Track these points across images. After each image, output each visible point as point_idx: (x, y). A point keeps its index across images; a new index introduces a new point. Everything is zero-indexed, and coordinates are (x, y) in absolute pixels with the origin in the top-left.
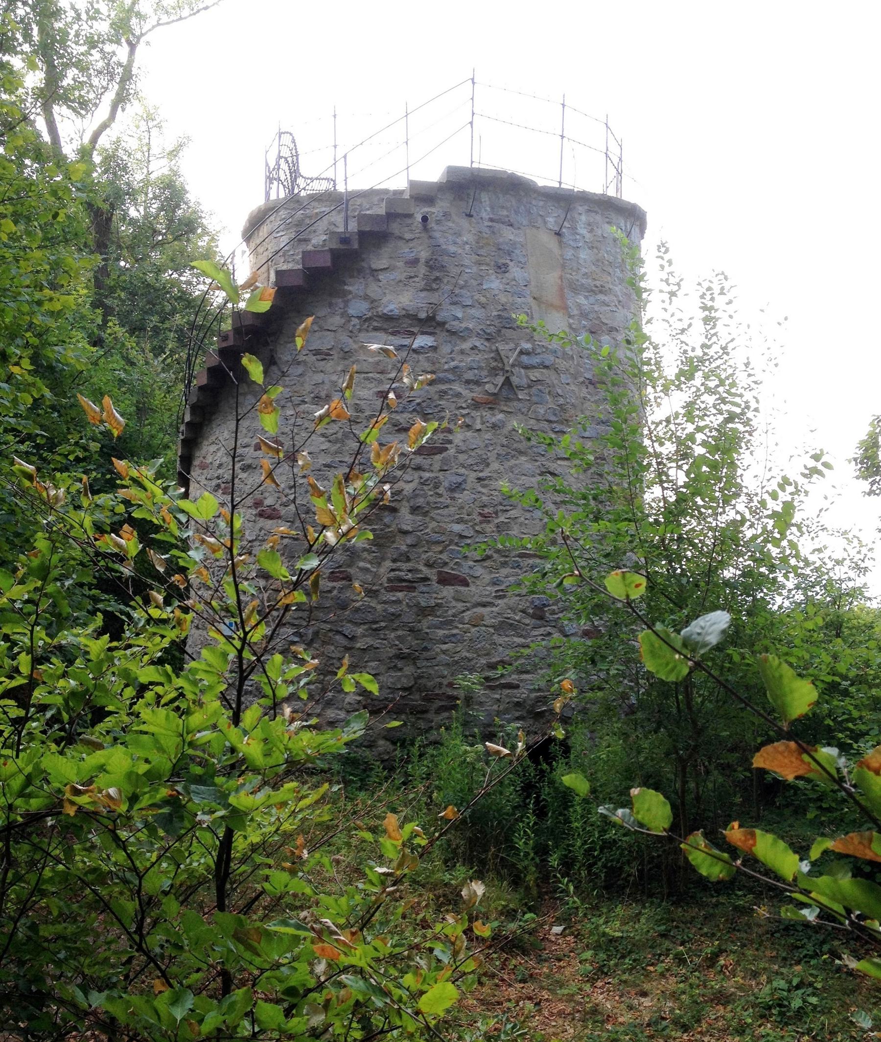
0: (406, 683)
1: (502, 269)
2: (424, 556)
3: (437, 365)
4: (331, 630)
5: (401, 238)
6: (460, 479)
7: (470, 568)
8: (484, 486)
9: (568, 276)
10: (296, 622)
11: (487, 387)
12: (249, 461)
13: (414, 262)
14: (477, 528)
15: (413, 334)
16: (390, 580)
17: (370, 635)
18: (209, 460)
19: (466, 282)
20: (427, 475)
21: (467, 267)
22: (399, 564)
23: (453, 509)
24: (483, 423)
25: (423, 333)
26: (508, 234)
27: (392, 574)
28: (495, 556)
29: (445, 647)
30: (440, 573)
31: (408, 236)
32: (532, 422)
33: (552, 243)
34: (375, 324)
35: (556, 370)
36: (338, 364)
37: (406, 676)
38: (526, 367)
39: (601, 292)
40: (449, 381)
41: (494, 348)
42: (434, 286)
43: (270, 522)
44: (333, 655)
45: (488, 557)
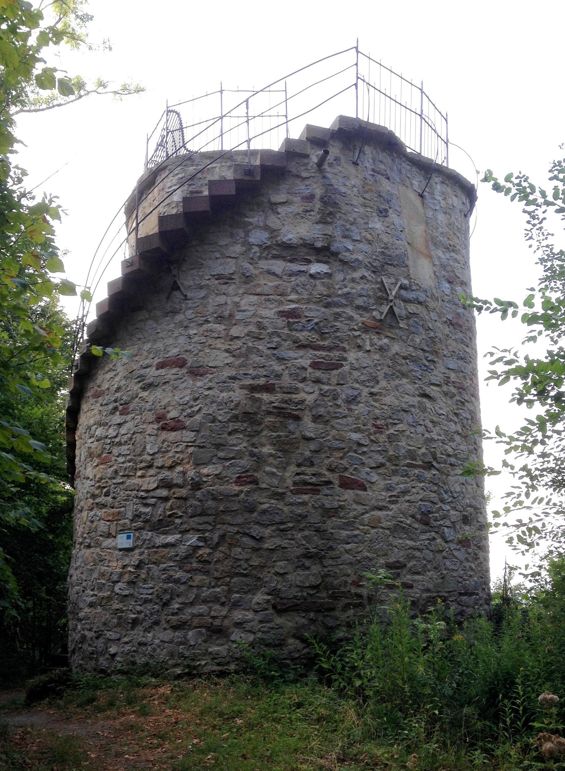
0: (313, 581)
1: (383, 213)
2: (327, 462)
3: (332, 290)
4: (238, 533)
5: (298, 176)
6: (356, 393)
7: (368, 474)
8: (376, 401)
10: (201, 527)
11: (374, 313)
12: (151, 380)
13: (310, 198)
14: (372, 437)
15: (309, 262)
16: (295, 483)
17: (278, 536)
18: (105, 386)
19: (355, 219)
20: (326, 388)
21: (355, 206)
22: (303, 468)
23: (350, 419)
24: (372, 345)
25: (319, 261)
26: (386, 186)
27: (297, 478)
28: (388, 464)
29: (348, 547)
31: (304, 174)
32: (411, 349)
33: (417, 201)
34: (275, 252)
36: (239, 288)
38: (406, 301)
39: (453, 251)
41: (379, 280)
42: (329, 220)
43: (174, 434)
44: (241, 557)
45: (382, 465)
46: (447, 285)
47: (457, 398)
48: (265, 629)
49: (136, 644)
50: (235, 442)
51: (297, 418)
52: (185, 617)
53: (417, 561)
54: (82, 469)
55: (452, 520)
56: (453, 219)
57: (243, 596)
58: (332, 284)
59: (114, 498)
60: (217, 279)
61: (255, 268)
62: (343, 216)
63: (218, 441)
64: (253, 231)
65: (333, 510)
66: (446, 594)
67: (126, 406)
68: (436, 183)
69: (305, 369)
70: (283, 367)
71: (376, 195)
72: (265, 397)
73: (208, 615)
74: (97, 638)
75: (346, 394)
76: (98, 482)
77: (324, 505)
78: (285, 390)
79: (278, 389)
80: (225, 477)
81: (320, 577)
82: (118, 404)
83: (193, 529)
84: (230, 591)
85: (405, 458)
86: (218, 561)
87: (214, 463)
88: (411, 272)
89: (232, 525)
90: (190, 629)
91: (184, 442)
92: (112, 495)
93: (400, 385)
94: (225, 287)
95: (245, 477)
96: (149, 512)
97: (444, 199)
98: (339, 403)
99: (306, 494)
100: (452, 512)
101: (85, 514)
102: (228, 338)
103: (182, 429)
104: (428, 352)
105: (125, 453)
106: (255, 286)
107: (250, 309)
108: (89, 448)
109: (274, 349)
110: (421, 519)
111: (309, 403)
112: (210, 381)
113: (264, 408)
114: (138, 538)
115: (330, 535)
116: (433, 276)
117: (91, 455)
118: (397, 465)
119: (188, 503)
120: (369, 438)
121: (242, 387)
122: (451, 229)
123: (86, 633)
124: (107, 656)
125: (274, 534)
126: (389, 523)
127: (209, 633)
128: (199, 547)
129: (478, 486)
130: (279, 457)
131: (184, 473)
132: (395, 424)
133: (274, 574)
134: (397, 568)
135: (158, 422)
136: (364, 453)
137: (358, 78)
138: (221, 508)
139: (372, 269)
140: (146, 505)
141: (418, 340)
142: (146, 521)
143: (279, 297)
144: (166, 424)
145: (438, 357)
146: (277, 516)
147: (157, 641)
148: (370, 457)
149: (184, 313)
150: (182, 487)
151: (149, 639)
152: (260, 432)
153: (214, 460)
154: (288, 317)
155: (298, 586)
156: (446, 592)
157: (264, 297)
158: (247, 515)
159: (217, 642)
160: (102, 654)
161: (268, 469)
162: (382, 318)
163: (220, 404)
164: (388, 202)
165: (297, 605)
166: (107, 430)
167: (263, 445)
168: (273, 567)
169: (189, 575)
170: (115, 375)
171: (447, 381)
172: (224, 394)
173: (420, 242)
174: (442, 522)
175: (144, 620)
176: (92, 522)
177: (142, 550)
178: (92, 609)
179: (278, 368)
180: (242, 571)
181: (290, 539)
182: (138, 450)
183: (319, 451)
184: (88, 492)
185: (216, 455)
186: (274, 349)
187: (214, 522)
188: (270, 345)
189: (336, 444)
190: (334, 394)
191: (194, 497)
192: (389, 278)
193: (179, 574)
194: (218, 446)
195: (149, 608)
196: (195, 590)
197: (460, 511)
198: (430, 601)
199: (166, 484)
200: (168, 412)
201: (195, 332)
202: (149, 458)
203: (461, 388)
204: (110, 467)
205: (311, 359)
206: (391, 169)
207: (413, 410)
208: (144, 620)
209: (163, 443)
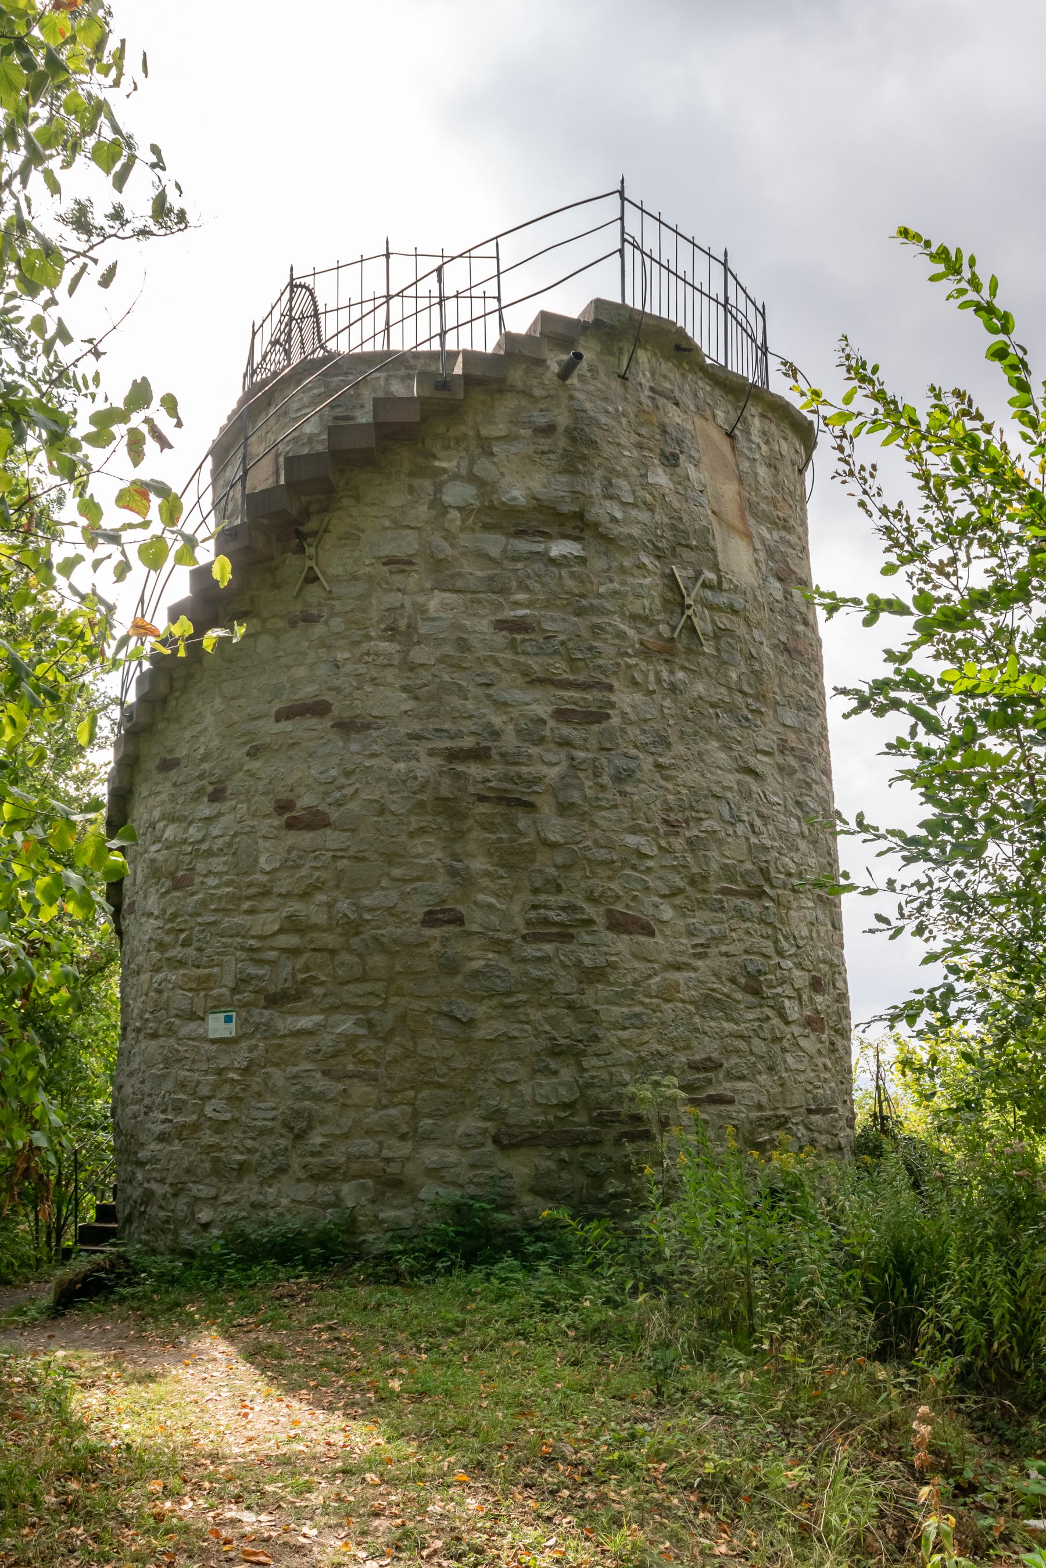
0: (566, 1095)
1: (671, 461)
4: (429, 1011)
8: (667, 778)
10: (360, 1002)
12: (268, 740)
13: (549, 430)
14: (663, 843)
21: (624, 447)
22: (543, 897)
23: (625, 811)
24: (659, 681)
27: (533, 915)
29: (625, 1035)
32: (723, 690)
33: (725, 445)
35: (747, 620)
38: (712, 608)
39: (785, 528)
40: (606, 612)
44: (434, 1055)
45: (680, 891)
46: (778, 585)
47: (799, 775)
48: (482, 1180)
49: (248, 1207)
50: (421, 850)
52: (338, 1157)
53: (740, 1057)
54: (139, 898)
55: (797, 986)
56: (781, 476)
58: (588, 576)
59: (200, 950)
60: (385, 564)
61: (452, 546)
62: (606, 463)
64: (450, 485)
66: (786, 1113)
68: (753, 416)
69: (543, 722)
70: (505, 718)
72: (474, 770)
73: (377, 1156)
74: (175, 1195)
75: (617, 767)
77: (581, 962)
81: (576, 1089)
82: (205, 782)
83: (346, 1005)
85: (719, 878)
86: (395, 1061)
87: (383, 888)
90: (347, 1178)
91: (328, 850)
92: (196, 944)
94: (398, 578)
96: (264, 975)
97: (767, 443)
98: (604, 782)
99: (550, 941)
100: (797, 973)
101: (145, 977)
103: (325, 826)
104: (751, 696)
105: (219, 869)
106: (452, 576)
107: (443, 615)
108: (153, 861)
109: (487, 685)
112: (375, 742)
113: (471, 789)
115: (594, 1015)
116: (755, 568)
118: (705, 891)
119: (338, 960)
121: (432, 753)
122: (778, 492)
123: (154, 1186)
125: (494, 1013)
128: (357, 1038)
129: (834, 926)
130: (501, 877)
131: (330, 906)
132: (701, 819)
134: (706, 1069)
136: (649, 869)
137: (623, 240)
141: (734, 676)
143: (495, 597)
144: (295, 817)
145: (766, 705)
147: (285, 1201)
149: (326, 623)
150: (325, 931)
153: (384, 883)
154: (511, 631)
155: (539, 1105)
156: (787, 1109)
157: (470, 596)
159: (395, 1203)
160: (184, 1223)
161: (481, 897)
166: (186, 829)
171: (783, 748)
172: (402, 766)
173: (731, 510)
174: (779, 990)
175: (260, 1164)
176: (159, 992)
177: (254, 1042)
178: (164, 1144)
180: (436, 1079)
181: (521, 1022)
183: (571, 866)
184: (151, 939)
186: (487, 685)
189: (602, 854)
192: (685, 568)
193: (320, 1084)
195: (269, 1142)
196: (353, 1114)
198: (762, 1126)
199: (293, 925)
200: (299, 797)
201: (347, 655)
203: (805, 760)
204: (193, 894)
205: (552, 704)
206: (681, 390)
208: (260, 1164)
209: (289, 851)
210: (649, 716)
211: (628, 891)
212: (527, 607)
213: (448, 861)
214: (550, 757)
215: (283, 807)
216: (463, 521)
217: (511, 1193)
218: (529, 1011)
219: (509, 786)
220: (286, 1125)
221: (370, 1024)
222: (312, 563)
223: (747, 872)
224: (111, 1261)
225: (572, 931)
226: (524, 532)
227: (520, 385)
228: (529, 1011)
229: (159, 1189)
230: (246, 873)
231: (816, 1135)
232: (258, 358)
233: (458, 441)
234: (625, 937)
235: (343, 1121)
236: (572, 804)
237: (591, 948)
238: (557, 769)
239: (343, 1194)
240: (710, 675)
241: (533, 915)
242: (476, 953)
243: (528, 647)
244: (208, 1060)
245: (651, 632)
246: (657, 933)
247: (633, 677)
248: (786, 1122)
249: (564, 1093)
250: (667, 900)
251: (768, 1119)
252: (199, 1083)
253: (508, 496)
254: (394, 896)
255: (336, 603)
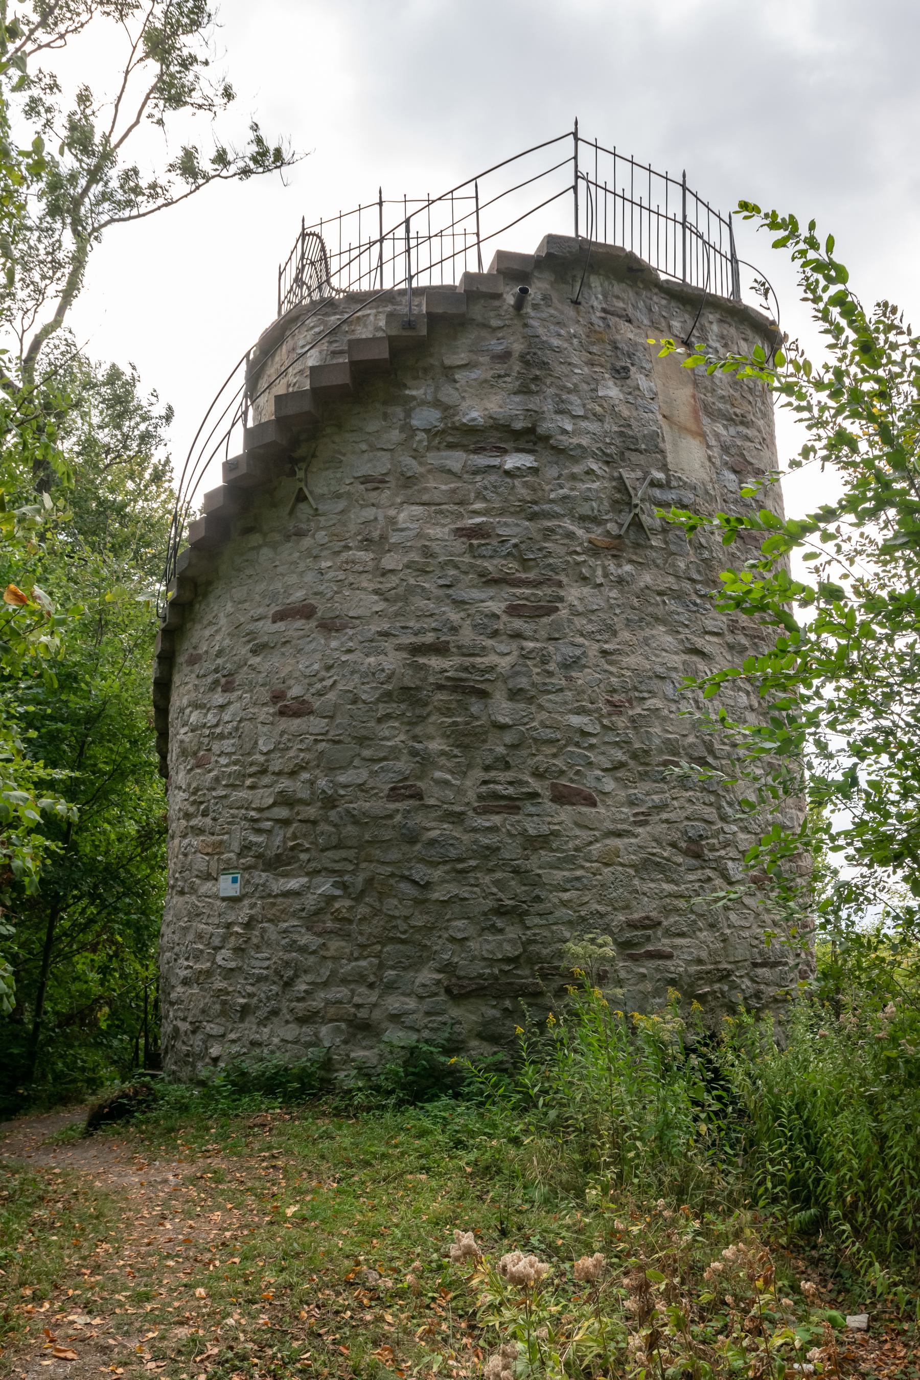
0: (510, 951)
1: (621, 374)
2: (530, 762)
3: (540, 493)
4: (392, 875)
5: (485, 326)
6: (578, 652)
7: (598, 779)
8: (610, 663)
9: (703, 396)
10: (337, 867)
11: (609, 526)
12: (265, 639)
13: (505, 356)
15: (504, 451)
16: (480, 797)
18: (204, 648)
20: (530, 645)
21: (576, 366)
22: (493, 774)
23: (569, 693)
24: (606, 575)
25: (519, 450)
26: (627, 332)
27: (484, 789)
28: (632, 763)
29: (566, 896)
30: (554, 786)
31: (495, 323)
32: (671, 579)
34: (450, 439)
36: (397, 495)
37: (510, 941)
40: (557, 516)
42: (533, 387)
43: (297, 721)
45: (621, 765)
46: (733, 477)
47: (751, 653)
48: (435, 1025)
51: (483, 694)
52: (316, 1003)
53: (680, 915)
55: (741, 849)
57: (402, 974)
58: (539, 484)
59: (214, 819)
60: (362, 483)
61: (421, 464)
62: (556, 381)
63: (364, 732)
64: (418, 410)
65: (540, 839)
66: (729, 967)
67: (230, 679)
68: (711, 323)
69: (497, 617)
70: (462, 614)
71: (609, 347)
72: (435, 662)
73: (350, 1002)
74: (194, 1032)
75: (563, 654)
76: (194, 793)
78: (464, 650)
79: (454, 650)
80: (373, 788)
81: (519, 945)
83: (326, 869)
84: (381, 966)
85: (661, 752)
86: (363, 919)
88: (668, 460)
89: (383, 863)
91: (311, 734)
92: (212, 815)
93: (653, 636)
94: (374, 494)
95: (402, 787)
97: (725, 346)
98: (551, 669)
99: (498, 813)
100: (742, 836)
101: (176, 841)
102: (378, 573)
103: (309, 714)
104: (700, 582)
105: (229, 750)
106: (419, 491)
107: (411, 526)
109: (448, 586)
110: (688, 848)
111: (503, 671)
112: (351, 639)
113: (431, 680)
114: (248, 882)
115: (537, 878)
116: (708, 464)
117: (184, 752)
118: (647, 764)
120: (601, 723)
121: (399, 648)
122: (736, 390)
123: (179, 1024)
124: (207, 1060)
125: (448, 877)
126: (634, 857)
127: (350, 1030)
128: (334, 898)
130: (456, 756)
131: (312, 783)
132: (644, 699)
133: (447, 940)
134: (645, 927)
135: (275, 703)
136: (592, 747)
137: (577, 177)
138: (367, 837)
139: (605, 458)
140: (259, 831)
141: (682, 565)
142: (258, 857)
143: (456, 507)
144: (286, 706)
146: (451, 849)
147: (276, 1040)
148: (603, 753)
150: (308, 805)
151: (265, 1037)
152: (425, 718)
153: (356, 762)
154: (469, 537)
155: (485, 959)
156: (730, 963)
157: (434, 508)
158: (405, 848)
159: (364, 1044)
160: (201, 1057)
161: (438, 774)
162: (622, 533)
163: (364, 675)
164: (630, 357)
165: (484, 988)
166: (206, 715)
167: (431, 738)
168: (446, 929)
169: (321, 941)
170: (217, 631)
172: (371, 660)
173: (683, 414)
174: (722, 853)
176: (186, 855)
177: (254, 900)
179: (455, 616)
180: (398, 935)
181: (472, 885)
182: (248, 746)
184: (180, 809)
185: (359, 755)
186: (448, 586)
187: (357, 858)
188: (441, 582)
189: (549, 734)
190: (544, 655)
191: (326, 820)
192: (633, 470)
193: (305, 938)
194: (362, 741)
195: (264, 988)
196: (330, 964)
197: (756, 834)
198: (702, 978)
199: (285, 800)
200: (289, 688)
201: (329, 564)
202: (262, 759)
204: (210, 771)
205: (506, 600)
206: (635, 307)
207: (674, 675)
209: (281, 736)
210: (595, 607)
211: (571, 767)
212: (484, 515)
213: (410, 743)
214: (503, 648)
215: (277, 697)
216: (429, 442)
217: (460, 1038)
218: (478, 875)
219: (464, 675)
220: (277, 972)
221: (344, 886)
222: (302, 485)
223: (691, 745)
224: (135, 1088)
225: (518, 803)
226: (484, 449)
227: (479, 318)
228: (478, 875)
229: (184, 1026)
230: (249, 754)
231: (762, 987)
232: (282, 298)
233: (426, 370)
234: (568, 808)
235: (323, 970)
236: (521, 690)
237: (535, 818)
238: (508, 659)
239: (321, 1035)
240: (657, 566)
241: (484, 789)
242: (433, 824)
243: (484, 551)
244: (220, 915)
245: (599, 530)
246: (599, 804)
247: (581, 573)
248: (729, 975)
249: (509, 948)
250: (610, 773)
251: (707, 973)
252: (212, 935)
253: (468, 417)
254: (364, 774)
255: (322, 518)
